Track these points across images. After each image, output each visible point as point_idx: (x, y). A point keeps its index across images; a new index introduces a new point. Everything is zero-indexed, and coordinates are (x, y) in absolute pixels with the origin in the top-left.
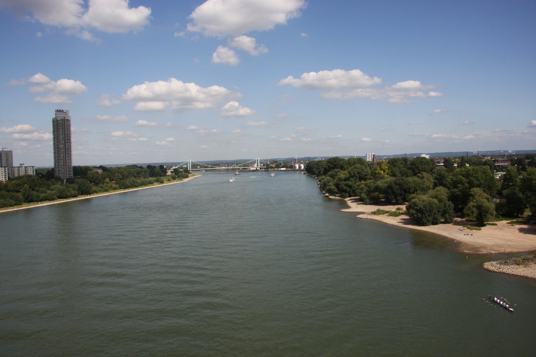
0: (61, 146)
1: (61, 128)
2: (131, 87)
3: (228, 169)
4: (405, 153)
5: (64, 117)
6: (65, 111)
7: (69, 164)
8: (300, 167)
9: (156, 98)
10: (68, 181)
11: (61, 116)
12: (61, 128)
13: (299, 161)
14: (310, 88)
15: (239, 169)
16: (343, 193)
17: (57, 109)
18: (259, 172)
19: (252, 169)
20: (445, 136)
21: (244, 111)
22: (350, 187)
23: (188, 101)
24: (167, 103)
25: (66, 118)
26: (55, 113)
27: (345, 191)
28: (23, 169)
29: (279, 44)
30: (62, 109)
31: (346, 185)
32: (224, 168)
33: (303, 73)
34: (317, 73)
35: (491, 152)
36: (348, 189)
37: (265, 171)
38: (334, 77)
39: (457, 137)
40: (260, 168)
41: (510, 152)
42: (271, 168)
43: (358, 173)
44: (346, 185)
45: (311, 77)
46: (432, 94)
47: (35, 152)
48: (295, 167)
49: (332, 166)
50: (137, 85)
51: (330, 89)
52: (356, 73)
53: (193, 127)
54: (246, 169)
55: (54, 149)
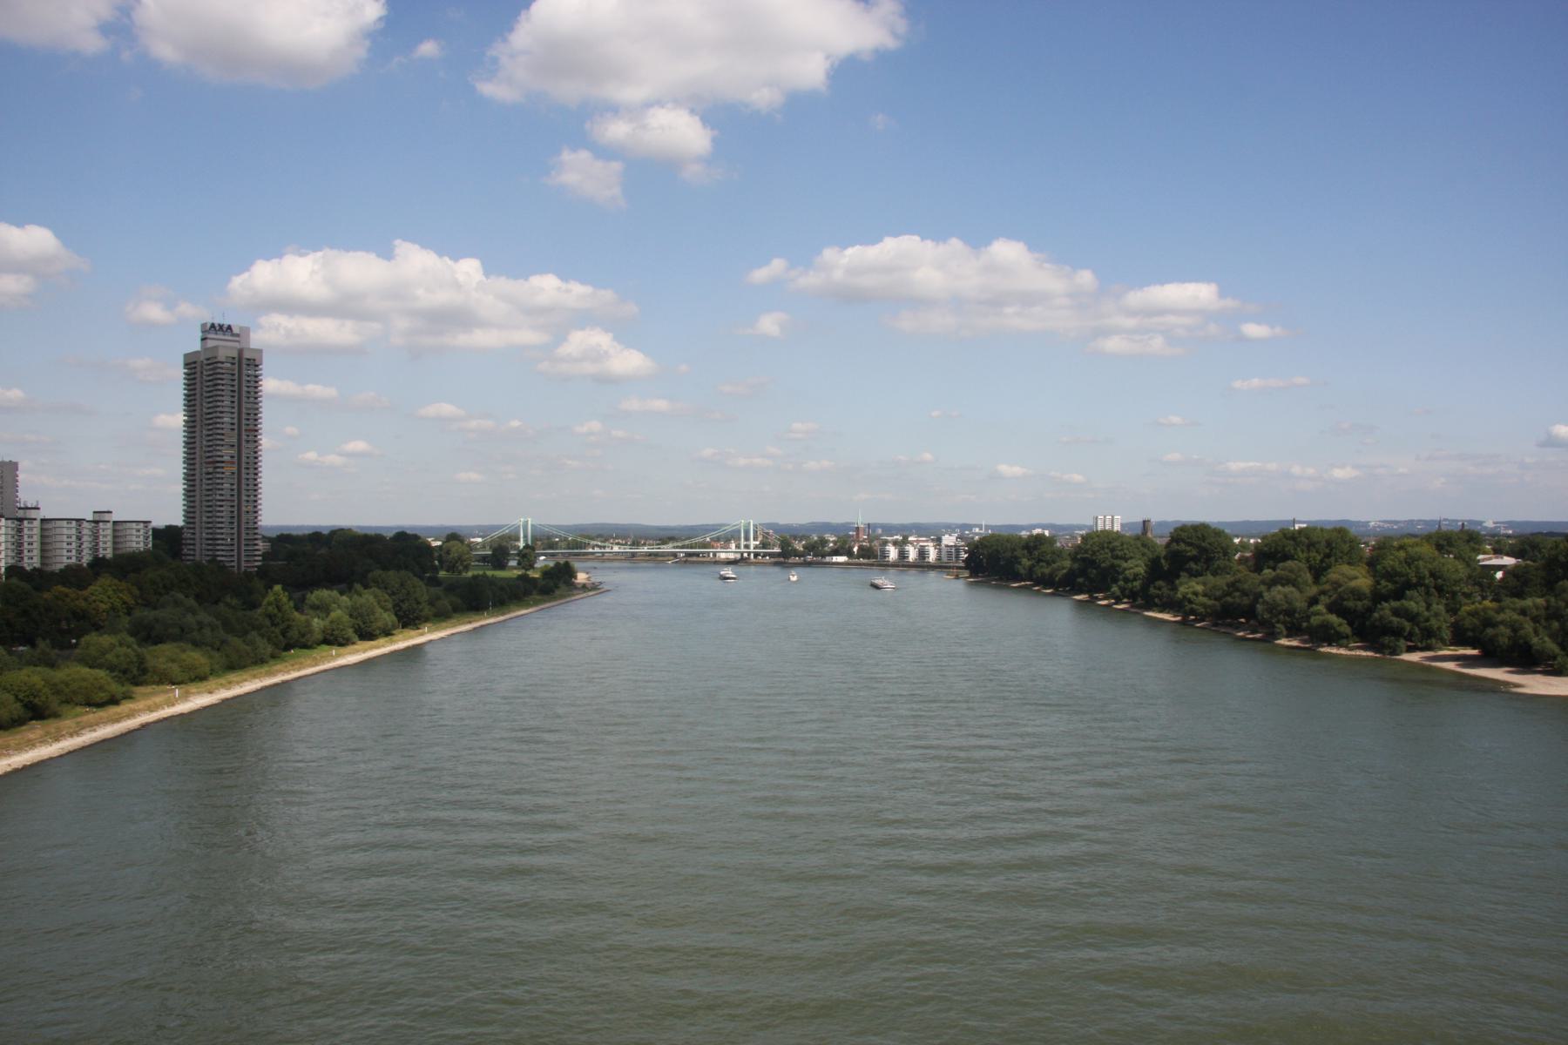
0: (227, 453)
1: (222, 391)
2: (245, 266)
3: (633, 555)
4: (1138, 518)
5: (241, 352)
6: (236, 330)
7: (251, 517)
8: (922, 553)
9: (341, 307)
10: (229, 583)
11: (225, 348)
12: (222, 391)
13: (950, 529)
14: (850, 297)
15: (675, 555)
16: (1386, 640)
17: (210, 321)
18: (753, 569)
19: (723, 556)
20: (1273, 466)
21: (629, 361)
22: (1412, 617)
23: (457, 318)
24: (376, 326)
25: (246, 355)
26: (199, 335)
27: (1397, 633)
28: (106, 532)
29: (793, 153)
30: (226, 323)
31: (1396, 612)
32: (616, 549)
33: (229, 281)
34: (487, 273)
35: (1426, 522)
36: (1407, 625)
37: (776, 564)
38: (917, 260)
39: (1310, 471)
40: (756, 555)
41: (1489, 524)
42: (796, 554)
43: (1432, 575)
44: (1396, 612)
45: (847, 261)
46: (1253, 330)
47: (119, 472)
48: (884, 554)
49: (1194, 552)
50: (268, 259)
51: (919, 302)
52: (1007, 251)
53: (447, 409)
54: (697, 555)
55: (190, 460)
